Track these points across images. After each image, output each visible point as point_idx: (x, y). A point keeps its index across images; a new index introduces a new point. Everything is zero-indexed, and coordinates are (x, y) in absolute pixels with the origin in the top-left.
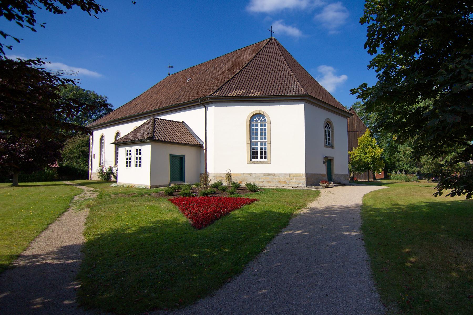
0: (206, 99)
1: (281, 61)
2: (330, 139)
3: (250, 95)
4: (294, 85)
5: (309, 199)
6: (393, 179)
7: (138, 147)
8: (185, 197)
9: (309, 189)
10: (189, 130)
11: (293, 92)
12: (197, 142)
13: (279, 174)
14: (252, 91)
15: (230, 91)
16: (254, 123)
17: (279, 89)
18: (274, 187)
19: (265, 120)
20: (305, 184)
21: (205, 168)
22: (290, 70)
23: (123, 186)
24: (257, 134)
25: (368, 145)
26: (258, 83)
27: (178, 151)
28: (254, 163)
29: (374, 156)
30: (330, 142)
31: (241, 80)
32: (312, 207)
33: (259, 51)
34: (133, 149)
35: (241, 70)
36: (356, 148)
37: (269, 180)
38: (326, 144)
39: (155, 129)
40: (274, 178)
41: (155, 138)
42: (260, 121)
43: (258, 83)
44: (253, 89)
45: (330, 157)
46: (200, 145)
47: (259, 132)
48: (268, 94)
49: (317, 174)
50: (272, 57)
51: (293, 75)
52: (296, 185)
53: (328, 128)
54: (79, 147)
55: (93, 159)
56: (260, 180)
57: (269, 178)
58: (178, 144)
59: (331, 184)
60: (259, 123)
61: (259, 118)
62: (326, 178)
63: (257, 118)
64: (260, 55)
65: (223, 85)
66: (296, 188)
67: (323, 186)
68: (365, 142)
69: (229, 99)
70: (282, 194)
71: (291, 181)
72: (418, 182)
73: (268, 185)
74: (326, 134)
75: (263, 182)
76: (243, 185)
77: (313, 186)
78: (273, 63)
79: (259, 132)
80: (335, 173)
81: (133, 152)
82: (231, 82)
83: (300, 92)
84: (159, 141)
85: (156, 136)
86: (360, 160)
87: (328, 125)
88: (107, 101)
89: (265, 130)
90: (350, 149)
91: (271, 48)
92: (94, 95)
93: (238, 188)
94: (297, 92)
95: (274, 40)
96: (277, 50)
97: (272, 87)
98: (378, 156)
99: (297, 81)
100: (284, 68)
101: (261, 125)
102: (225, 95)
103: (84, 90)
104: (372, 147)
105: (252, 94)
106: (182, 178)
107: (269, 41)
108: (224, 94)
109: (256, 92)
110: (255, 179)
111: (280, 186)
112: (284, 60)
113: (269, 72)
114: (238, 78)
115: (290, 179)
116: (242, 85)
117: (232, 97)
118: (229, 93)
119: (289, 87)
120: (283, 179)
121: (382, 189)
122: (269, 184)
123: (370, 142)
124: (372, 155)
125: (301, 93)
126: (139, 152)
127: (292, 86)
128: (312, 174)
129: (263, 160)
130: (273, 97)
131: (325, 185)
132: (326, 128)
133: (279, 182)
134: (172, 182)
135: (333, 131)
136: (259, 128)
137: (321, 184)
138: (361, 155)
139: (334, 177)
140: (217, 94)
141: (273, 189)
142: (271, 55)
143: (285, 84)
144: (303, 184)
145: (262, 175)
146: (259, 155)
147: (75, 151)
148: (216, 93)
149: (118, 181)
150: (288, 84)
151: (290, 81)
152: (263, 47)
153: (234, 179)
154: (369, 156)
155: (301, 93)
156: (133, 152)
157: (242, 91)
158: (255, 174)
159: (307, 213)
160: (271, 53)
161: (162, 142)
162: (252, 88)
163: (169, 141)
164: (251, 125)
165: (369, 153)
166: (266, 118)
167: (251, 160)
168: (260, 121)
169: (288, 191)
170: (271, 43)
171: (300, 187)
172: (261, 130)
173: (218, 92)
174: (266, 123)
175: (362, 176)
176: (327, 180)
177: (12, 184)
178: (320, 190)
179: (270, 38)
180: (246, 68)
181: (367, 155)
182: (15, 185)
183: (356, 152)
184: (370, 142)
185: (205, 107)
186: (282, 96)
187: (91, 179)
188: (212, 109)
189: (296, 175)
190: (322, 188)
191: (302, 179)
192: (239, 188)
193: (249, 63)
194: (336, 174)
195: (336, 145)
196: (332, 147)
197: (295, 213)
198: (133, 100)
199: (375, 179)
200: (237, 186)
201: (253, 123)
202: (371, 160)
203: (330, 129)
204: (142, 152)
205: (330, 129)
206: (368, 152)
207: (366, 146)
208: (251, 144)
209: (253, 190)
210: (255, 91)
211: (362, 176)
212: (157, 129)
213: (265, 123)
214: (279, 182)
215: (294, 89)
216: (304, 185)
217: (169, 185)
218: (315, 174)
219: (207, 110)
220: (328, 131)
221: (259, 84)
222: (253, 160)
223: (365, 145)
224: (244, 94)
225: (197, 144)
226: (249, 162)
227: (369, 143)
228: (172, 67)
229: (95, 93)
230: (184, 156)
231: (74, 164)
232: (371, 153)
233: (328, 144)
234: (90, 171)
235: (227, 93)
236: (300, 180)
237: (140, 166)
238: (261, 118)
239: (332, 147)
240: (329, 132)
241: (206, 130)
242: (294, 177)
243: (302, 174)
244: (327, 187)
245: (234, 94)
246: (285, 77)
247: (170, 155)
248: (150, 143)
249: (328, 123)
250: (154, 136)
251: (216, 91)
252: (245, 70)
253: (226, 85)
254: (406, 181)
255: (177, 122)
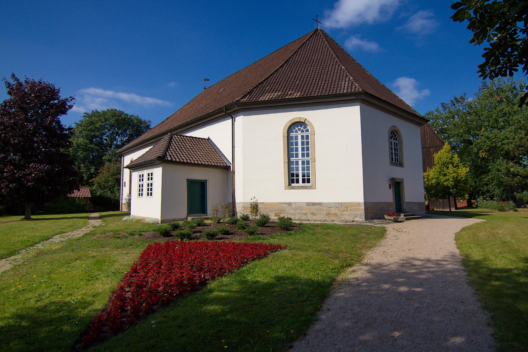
0: (232, 107)
1: (328, 54)
2: (397, 154)
3: (287, 97)
4: (346, 81)
5: (368, 244)
6: (481, 208)
7: (150, 171)
8: (182, 239)
9: (369, 224)
10: (215, 148)
11: (344, 89)
12: (223, 162)
13: (327, 203)
14: (289, 93)
15: (262, 94)
16: (293, 134)
17: (325, 87)
18: (320, 221)
19: (307, 131)
20: (364, 217)
21: (233, 196)
22: (340, 63)
23: (139, 221)
24: (297, 149)
25: (448, 164)
26: (297, 82)
27: (198, 174)
28: (293, 188)
29: (457, 177)
30: (397, 159)
31: (277, 80)
32: (373, 262)
33: (301, 45)
34: (145, 172)
35: (278, 69)
36: (431, 168)
37: (314, 212)
38: (392, 160)
39: (170, 147)
40: (320, 209)
41: (167, 158)
42: (301, 132)
43: (297, 82)
44: (291, 90)
45: (397, 179)
46: (227, 166)
47: (300, 146)
48: (311, 94)
49: (381, 203)
50: (317, 51)
51: (344, 69)
52: (350, 219)
53: (394, 139)
54: (114, 175)
55: (124, 187)
56: (302, 212)
57: (313, 209)
58: (198, 165)
59: (401, 217)
60: (299, 134)
61: (299, 128)
62: (393, 208)
63: (296, 129)
64: (302, 50)
65: (254, 88)
66: (351, 223)
67: (389, 220)
68: (444, 160)
69: (261, 104)
70: (328, 234)
71: (344, 213)
72: (516, 211)
73: (313, 218)
74: (392, 153)
75: (306, 214)
76: (273, 218)
77: (376, 220)
78: (319, 58)
79: (300, 146)
80: (406, 201)
81: (146, 177)
82: (264, 84)
83: (353, 89)
84: (172, 162)
85: (168, 156)
86: (438, 184)
87: (394, 134)
88: (150, 126)
89: (308, 143)
90: (425, 171)
91: (316, 41)
92: (137, 119)
93: (264, 224)
94: (349, 90)
95: (320, 31)
96: (324, 42)
97: (316, 86)
98: (462, 178)
99: (349, 75)
100: (332, 62)
101: (302, 137)
102: (256, 99)
103: (127, 115)
104: (453, 166)
105: (290, 96)
106: (203, 210)
107: (314, 33)
108: (254, 99)
109: (294, 93)
110: (296, 211)
111: (329, 220)
112: (332, 52)
113: (312, 68)
114: (273, 79)
115: (342, 210)
116: (277, 87)
117: (264, 102)
118: (261, 97)
119: (338, 84)
120: (333, 211)
121: (477, 224)
122: (314, 218)
123: (450, 159)
124: (454, 177)
125: (355, 90)
126: (150, 176)
127: (343, 83)
128: (374, 203)
129: (306, 184)
130: (317, 97)
131: (392, 218)
132: (391, 138)
133: (328, 214)
134: (191, 215)
135: (401, 143)
136: (300, 141)
137: (386, 217)
138: (438, 177)
139: (405, 207)
140: (245, 100)
141: (317, 226)
142: (316, 48)
143: (334, 81)
144: (360, 217)
145: (305, 205)
146: (300, 178)
147: (110, 179)
148: (245, 98)
149: (132, 213)
150: (337, 81)
151: (340, 77)
152: (307, 41)
153: (262, 210)
154: (450, 177)
155: (355, 90)
156: (146, 177)
157: (276, 94)
158: (295, 203)
159: (367, 280)
160: (316, 46)
161: (176, 163)
162: (290, 89)
163: (186, 161)
164: (289, 138)
165: (449, 174)
166: (308, 127)
167: (289, 185)
168: (301, 132)
169: (338, 229)
170: (316, 35)
171: (356, 221)
172: (303, 143)
173: (247, 97)
174: (309, 134)
175: (440, 204)
176: (395, 210)
177: (24, 217)
178: (385, 226)
179: (316, 28)
180: (284, 67)
181: (447, 177)
182: (28, 218)
183: (432, 173)
184: (450, 159)
185: (232, 118)
186: (329, 96)
187: (121, 210)
188: (240, 120)
189: (351, 204)
190: (388, 223)
191: (359, 210)
192: (267, 225)
193: (288, 60)
194: (408, 203)
195: (405, 163)
196: (401, 165)
197: (340, 278)
198: (166, 119)
199: (456, 208)
200: (264, 222)
201: (291, 134)
202: (453, 183)
203: (396, 140)
204: (154, 176)
205: (396, 140)
206: (449, 173)
207: (445, 165)
208: (289, 163)
209: (284, 228)
210: (293, 92)
211: (440, 204)
212: (173, 147)
213: (307, 134)
214: (328, 214)
215: (345, 87)
216: (362, 218)
217: (187, 218)
218: (378, 203)
219: (235, 121)
220: (394, 143)
221: (299, 83)
222: (293, 185)
223: (444, 164)
224: (279, 97)
225: (222, 165)
226: (287, 188)
227: (448, 160)
228: (208, 80)
229: (140, 117)
230: (206, 181)
231: (109, 194)
232: (452, 173)
233: (395, 161)
234: (121, 201)
235: (257, 97)
236: (357, 212)
237: (151, 195)
238: (302, 128)
239: (401, 165)
240: (396, 145)
241: (233, 147)
242: (347, 207)
243: (360, 203)
244: (396, 221)
245: (266, 97)
246: (334, 73)
247: (188, 180)
248: (161, 165)
249: (393, 133)
250: (167, 155)
251: (245, 96)
252: (283, 69)
253: (258, 88)
254: (500, 210)
255: (200, 139)
